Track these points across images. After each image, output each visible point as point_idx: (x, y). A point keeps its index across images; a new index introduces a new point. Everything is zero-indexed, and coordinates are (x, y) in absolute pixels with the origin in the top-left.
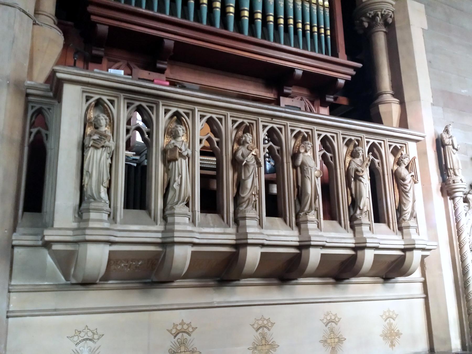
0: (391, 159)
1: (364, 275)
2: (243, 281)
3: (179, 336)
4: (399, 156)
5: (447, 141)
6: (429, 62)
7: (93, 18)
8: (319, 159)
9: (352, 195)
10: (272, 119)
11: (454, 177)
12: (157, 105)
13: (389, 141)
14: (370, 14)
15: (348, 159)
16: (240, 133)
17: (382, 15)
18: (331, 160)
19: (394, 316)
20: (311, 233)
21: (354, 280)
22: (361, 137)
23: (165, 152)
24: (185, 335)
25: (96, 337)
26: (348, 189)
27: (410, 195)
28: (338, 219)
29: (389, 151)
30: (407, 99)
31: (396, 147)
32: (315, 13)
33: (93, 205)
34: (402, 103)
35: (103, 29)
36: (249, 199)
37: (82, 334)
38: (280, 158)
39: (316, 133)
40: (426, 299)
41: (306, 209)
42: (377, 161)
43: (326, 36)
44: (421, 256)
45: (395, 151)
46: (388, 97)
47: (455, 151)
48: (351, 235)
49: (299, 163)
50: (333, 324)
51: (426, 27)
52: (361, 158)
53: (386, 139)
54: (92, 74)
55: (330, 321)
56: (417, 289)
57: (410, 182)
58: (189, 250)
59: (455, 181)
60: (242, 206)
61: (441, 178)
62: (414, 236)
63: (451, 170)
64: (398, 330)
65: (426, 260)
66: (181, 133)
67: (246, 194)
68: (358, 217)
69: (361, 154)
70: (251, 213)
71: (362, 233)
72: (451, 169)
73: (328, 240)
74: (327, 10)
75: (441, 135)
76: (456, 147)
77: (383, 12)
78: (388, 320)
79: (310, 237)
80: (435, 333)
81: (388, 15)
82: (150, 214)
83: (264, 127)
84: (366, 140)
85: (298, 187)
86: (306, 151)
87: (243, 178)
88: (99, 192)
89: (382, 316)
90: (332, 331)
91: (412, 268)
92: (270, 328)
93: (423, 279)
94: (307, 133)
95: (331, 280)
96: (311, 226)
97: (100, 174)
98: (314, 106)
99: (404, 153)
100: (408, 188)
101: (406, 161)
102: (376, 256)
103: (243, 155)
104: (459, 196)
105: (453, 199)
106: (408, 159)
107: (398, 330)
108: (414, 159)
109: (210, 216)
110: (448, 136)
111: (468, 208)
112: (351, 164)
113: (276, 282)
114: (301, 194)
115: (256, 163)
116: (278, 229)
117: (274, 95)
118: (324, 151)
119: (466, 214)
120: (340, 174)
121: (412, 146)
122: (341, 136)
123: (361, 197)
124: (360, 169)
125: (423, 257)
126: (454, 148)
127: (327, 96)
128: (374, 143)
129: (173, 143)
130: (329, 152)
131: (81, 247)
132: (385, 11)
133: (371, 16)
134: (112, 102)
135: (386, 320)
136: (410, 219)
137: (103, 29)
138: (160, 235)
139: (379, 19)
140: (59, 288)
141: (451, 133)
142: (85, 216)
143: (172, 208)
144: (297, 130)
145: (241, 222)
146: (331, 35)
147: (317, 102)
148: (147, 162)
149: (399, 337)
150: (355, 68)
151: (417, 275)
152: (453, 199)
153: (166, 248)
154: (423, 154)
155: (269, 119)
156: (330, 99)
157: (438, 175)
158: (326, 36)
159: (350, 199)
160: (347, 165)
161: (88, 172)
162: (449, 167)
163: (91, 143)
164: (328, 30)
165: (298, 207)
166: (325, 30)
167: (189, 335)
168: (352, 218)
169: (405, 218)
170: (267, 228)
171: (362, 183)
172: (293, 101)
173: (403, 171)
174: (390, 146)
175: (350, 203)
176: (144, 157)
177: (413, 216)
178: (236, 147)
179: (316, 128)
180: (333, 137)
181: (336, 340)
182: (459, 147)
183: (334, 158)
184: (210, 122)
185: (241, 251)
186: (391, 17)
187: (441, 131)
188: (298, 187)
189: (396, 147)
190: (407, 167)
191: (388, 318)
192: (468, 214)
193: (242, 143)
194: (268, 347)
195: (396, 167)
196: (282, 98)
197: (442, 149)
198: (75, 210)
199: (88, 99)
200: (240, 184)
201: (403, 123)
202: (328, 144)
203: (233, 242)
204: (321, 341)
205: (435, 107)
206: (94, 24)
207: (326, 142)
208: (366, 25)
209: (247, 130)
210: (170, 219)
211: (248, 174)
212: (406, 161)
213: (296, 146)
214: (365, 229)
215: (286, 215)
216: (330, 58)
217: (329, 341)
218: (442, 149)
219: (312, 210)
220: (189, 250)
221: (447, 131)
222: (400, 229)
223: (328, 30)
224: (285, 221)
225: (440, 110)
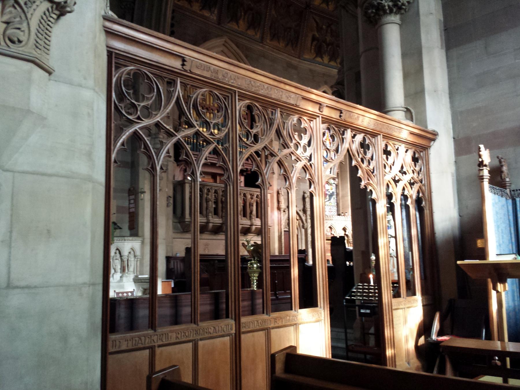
8: (242, 199)
21: (249, 234)
23: (206, 199)
54: (322, 147)
95: (243, 234)
96: (210, 217)
102: (256, 228)
104: (282, 210)
105: (280, 211)
138: (206, 220)
143: (208, 214)
152: (280, 211)
168: (250, 217)
187: (279, 188)
198: (509, 241)
221: (280, 189)
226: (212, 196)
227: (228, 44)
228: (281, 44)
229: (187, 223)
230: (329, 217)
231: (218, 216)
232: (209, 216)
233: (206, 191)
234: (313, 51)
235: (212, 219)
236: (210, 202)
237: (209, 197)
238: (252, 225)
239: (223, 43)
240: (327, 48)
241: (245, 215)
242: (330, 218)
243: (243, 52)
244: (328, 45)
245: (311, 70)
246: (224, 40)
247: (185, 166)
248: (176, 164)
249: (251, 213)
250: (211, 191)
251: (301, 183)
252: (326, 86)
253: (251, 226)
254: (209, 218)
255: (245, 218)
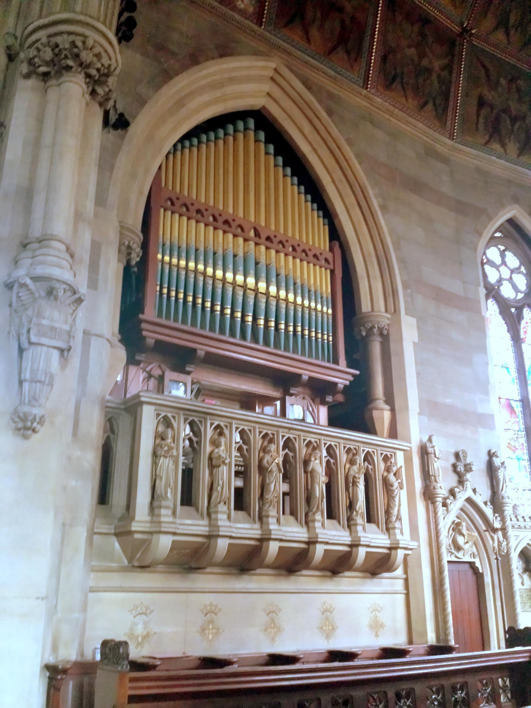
0: (382, 466)
1: (356, 570)
2: (259, 571)
3: (209, 615)
4: (389, 464)
5: (430, 450)
6: (418, 374)
7: (144, 333)
8: (324, 464)
9: (349, 498)
10: (290, 431)
11: (434, 483)
12: (206, 420)
13: (381, 450)
14: (368, 325)
15: (348, 466)
16: (266, 443)
17: (378, 327)
18: (334, 465)
19: (379, 609)
20: (318, 531)
21: (347, 574)
22: (358, 447)
23: (210, 459)
24: (213, 615)
25: (148, 612)
26: (347, 493)
27: (397, 499)
28: (337, 518)
29: (381, 459)
30: (397, 408)
31: (386, 455)
32: (320, 321)
33: (164, 503)
34: (393, 410)
35: (150, 342)
36: (271, 501)
37: (139, 609)
38: (294, 463)
39: (323, 442)
40: (407, 595)
41: (315, 510)
42: (370, 467)
43: (328, 341)
44: (403, 555)
45: (386, 459)
46: (381, 403)
47: (436, 459)
48: (347, 533)
49: (310, 469)
50: (328, 613)
51: (416, 340)
52: (358, 465)
53: (379, 448)
55: (326, 610)
56: (399, 585)
57: (397, 488)
58: (227, 541)
59: (436, 488)
60: (265, 506)
61: (424, 483)
62: (399, 537)
63: (432, 477)
64: (382, 623)
65: (408, 558)
66: (223, 443)
67: (269, 496)
68: (355, 518)
69: (358, 462)
70: (273, 512)
71: (357, 532)
72: (433, 476)
73: (330, 538)
74: (330, 317)
75: (425, 443)
76: (437, 456)
77: (379, 325)
78: (374, 612)
79: (317, 535)
80: (414, 626)
81: (383, 328)
82: (197, 510)
83: (283, 436)
84: (362, 448)
85: (307, 489)
86: (316, 460)
87: (268, 482)
88: (166, 493)
89: (369, 608)
90: (327, 619)
91: (396, 564)
92: (278, 613)
93: (404, 576)
94: (316, 442)
96: (318, 525)
97: (168, 478)
98: (314, 404)
99: (393, 461)
100: (395, 493)
101: (394, 469)
102: (367, 553)
103: (267, 462)
106: (396, 467)
107: (382, 623)
108: (401, 467)
109: (241, 514)
110: (431, 445)
111: (446, 512)
112: (350, 471)
113: (235, 571)
114: (310, 497)
115: (278, 469)
116: (291, 526)
117: (281, 394)
118: (328, 458)
119: (444, 518)
120: (341, 478)
121: (400, 455)
122: (342, 445)
123: (357, 501)
124: (357, 475)
125: (406, 556)
126: (435, 456)
127: (327, 396)
128: (368, 452)
129: (217, 453)
130: (331, 457)
131: (155, 536)
132: (381, 325)
133: (368, 328)
134: (174, 417)
135: (372, 613)
136: (396, 521)
137: (150, 342)
139: (375, 330)
140: (123, 570)
141: (434, 443)
142: (156, 511)
143: (216, 506)
144: (308, 439)
145: (265, 520)
146: (333, 341)
147: (318, 400)
148: (193, 465)
149: (383, 629)
150: (353, 375)
151: (399, 572)
153: (210, 540)
154: (408, 459)
155: (287, 430)
156: (329, 399)
157: (422, 480)
158: (328, 341)
159: (348, 501)
160: (347, 471)
161: (160, 475)
162: (431, 474)
163: (163, 453)
164: (330, 336)
165: (307, 508)
166: (328, 336)
167: (216, 614)
169: (391, 520)
170: (284, 526)
171: (358, 489)
172: (297, 400)
173: (392, 478)
174: (382, 454)
175: (348, 505)
176: (191, 461)
177: (399, 518)
178: (262, 454)
179: (323, 438)
180: (336, 446)
181: (331, 628)
182: (440, 456)
183: (336, 464)
184: (242, 433)
185: (265, 544)
186: (386, 329)
187: (425, 439)
188: (307, 489)
189: (386, 455)
190: (395, 474)
191: (375, 610)
192: (446, 517)
193: (267, 451)
194: (275, 630)
195: (385, 474)
196: (287, 398)
197: (426, 457)
199: (158, 415)
200: (263, 487)
201: (393, 434)
202: (331, 451)
203: (259, 537)
204: (318, 628)
205: (422, 417)
206: (144, 338)
207: (330, 449)
208: (364, 333)
209: (271, 441)
210: (213, 516)
211: (272, 479)
212: (394, 469)
213: (308, 454)
214: (360, 528)
215: (297, 515)
216: (331, 365)
217: (324, 628)
218: (426, 457)
219: (319, 511)
220: (227, 541)
221: (430, 440)
222: (388, 529)
223: (330, 336)
224: (297, 519)
225: (425, 419)
226: (229, 450)
227: (284, 78)
228: (410, 100)
229: (137, 536)
230: (521, 519)
231: (249, 515)
232: (217, 512)
233: (209, 433)
234: (481, 126)
235: (227, 523)
236: (224, 469)
237: (222, 450)
238: (354, 545)
239: (271, 73)
240: (513, 126)
241: (331, 514)
242: (518, 523)
243: (320, 102)
244: (514, 120)
245: (479, 171)
246: (273, 65)
247: (160, 367)
248: (122, 353)
249: (351, 506)
250: (227, 432)
251: (481, 430)
252: (516, 206)
253: (354, 549)
254: (217, 519)
255: (334, 522)
